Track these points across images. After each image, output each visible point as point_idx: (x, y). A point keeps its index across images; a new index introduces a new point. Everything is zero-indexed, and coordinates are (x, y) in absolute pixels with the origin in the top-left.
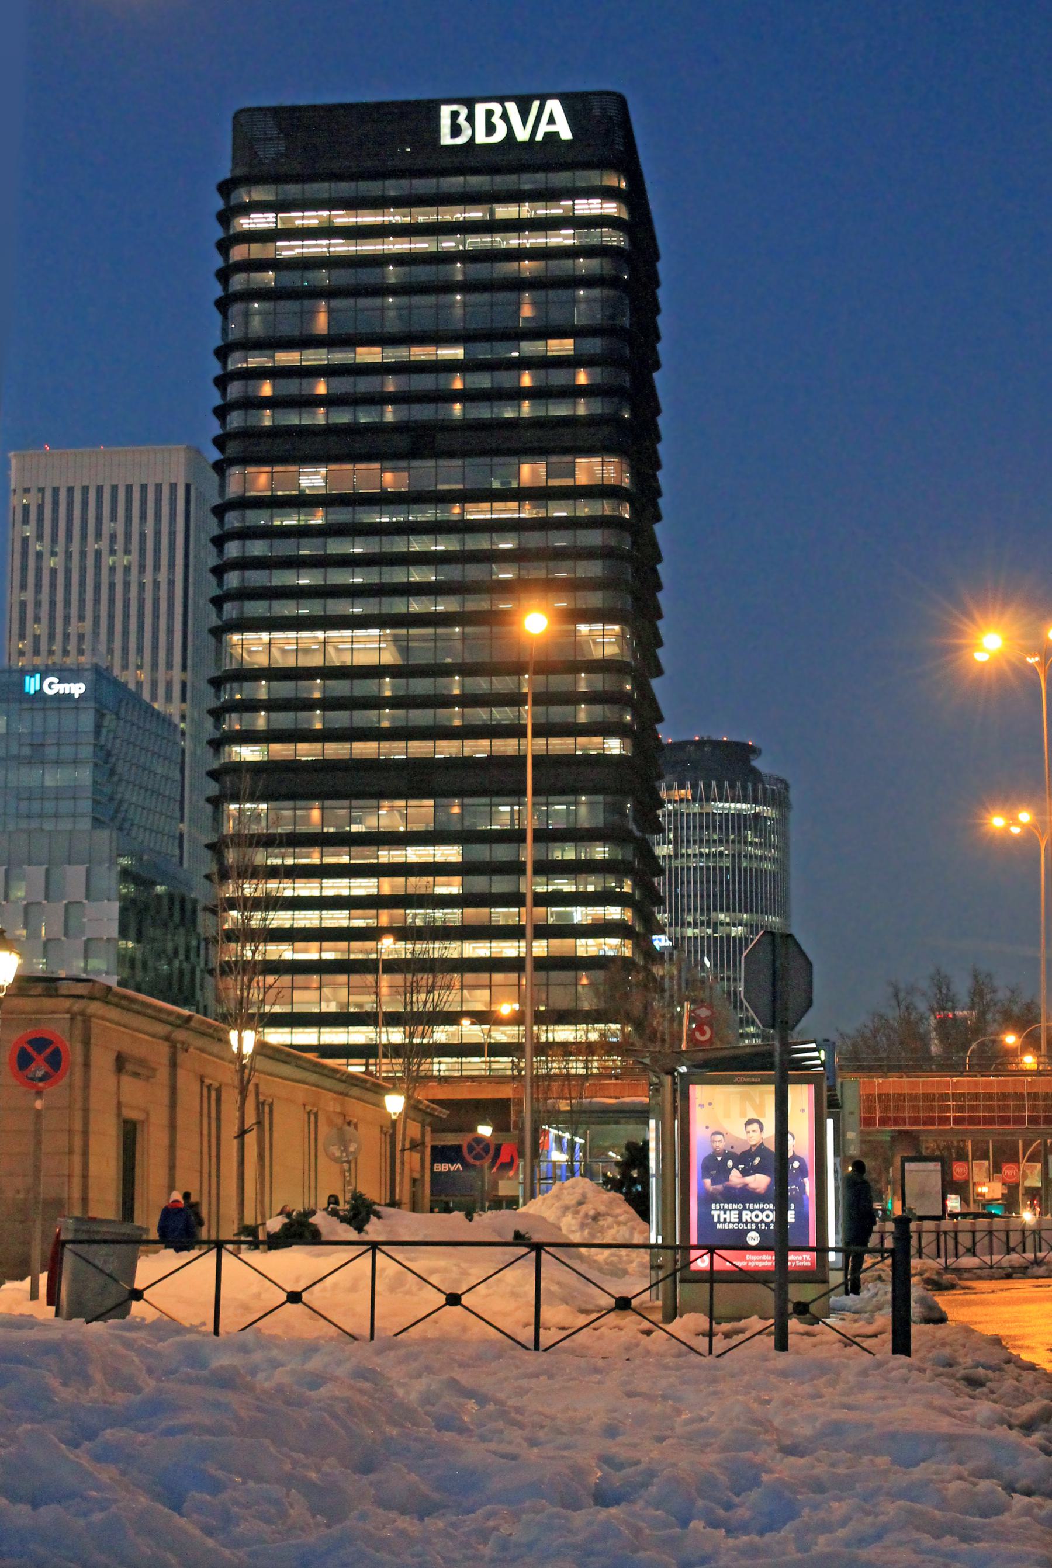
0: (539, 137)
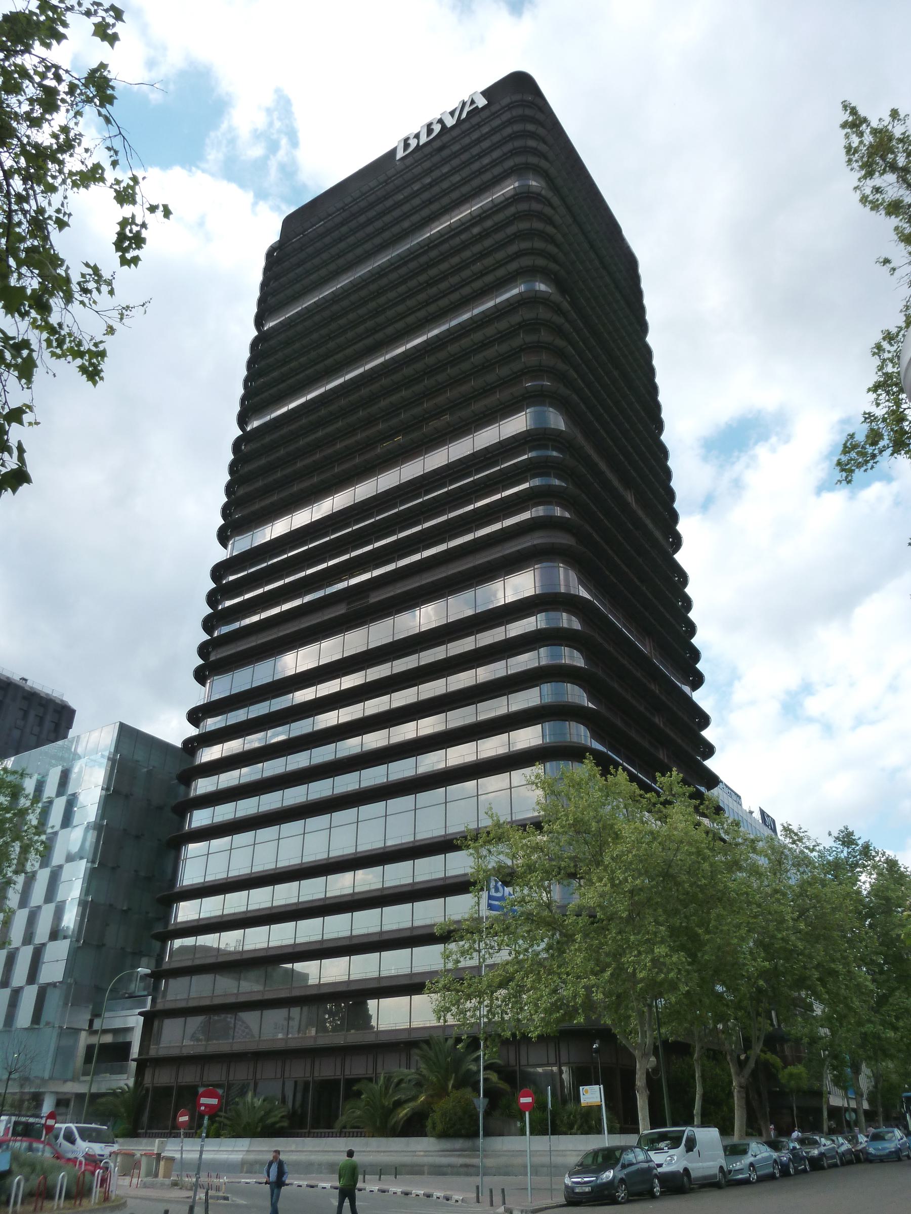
0: (464, 115)
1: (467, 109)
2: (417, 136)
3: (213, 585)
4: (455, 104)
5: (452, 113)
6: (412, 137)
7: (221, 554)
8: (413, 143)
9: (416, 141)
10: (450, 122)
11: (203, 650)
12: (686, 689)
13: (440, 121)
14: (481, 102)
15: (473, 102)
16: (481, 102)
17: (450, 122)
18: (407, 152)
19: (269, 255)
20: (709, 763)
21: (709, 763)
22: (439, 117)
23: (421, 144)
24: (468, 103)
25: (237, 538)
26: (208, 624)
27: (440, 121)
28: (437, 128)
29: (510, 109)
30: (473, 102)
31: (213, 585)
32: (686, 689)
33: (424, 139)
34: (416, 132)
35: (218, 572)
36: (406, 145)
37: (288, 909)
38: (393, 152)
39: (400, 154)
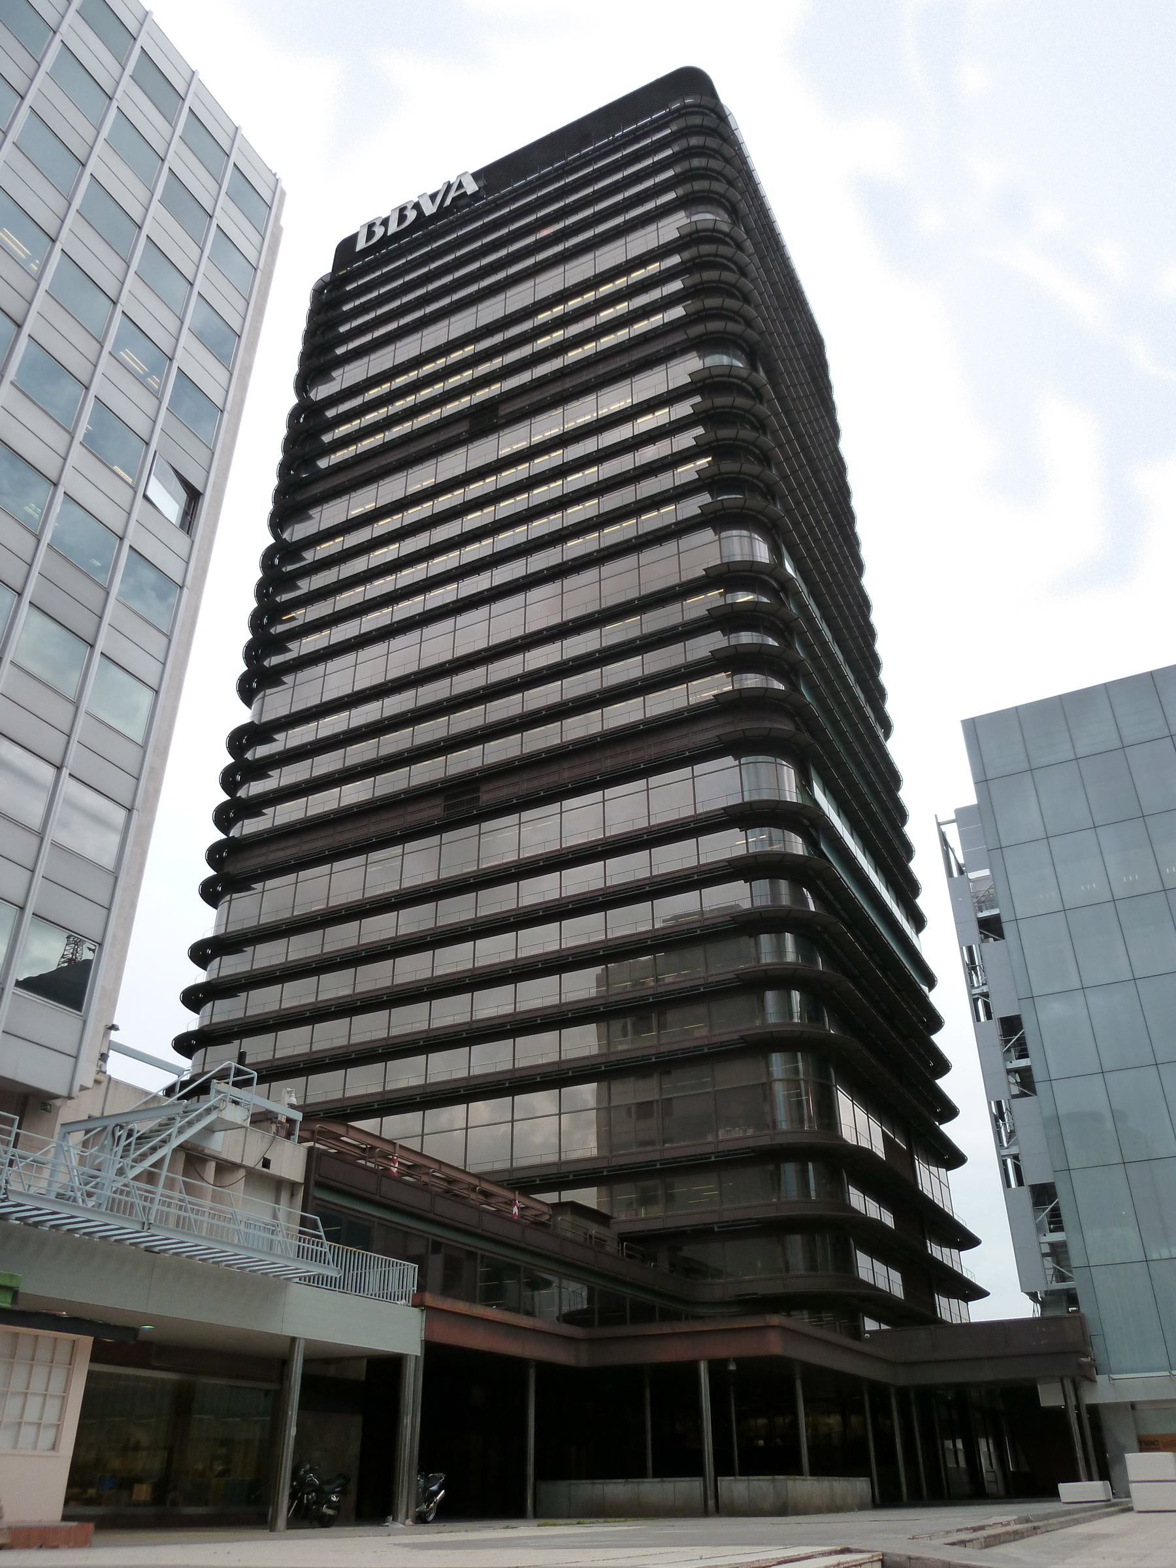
0: (448, 202)
1: (452, 194)
2: (385, 222)
3: (230, 760)
4: (438, 186)
5: (433, 197)
6: (378, 223)
7: (243, 715)
8: (379, 232)
9: (382, 229)
10: (429, 209)
11: (215, 855)
12: (925, 989)
13: (417, 206)
14: (471, 187)
15: (460, 186)
16: (471, 187)
17: (429, 209)
18: (403, 227)
19: (318, 292)
20: (947, 1128)
21: (947, 1128)
22: (416, 200)
23: (389, 234)
24: (455, 187)
25: (268, 691)
26: (223, 817)
27: (417, 206)
28: (411, 215)
29: (681, 116)
30: (460, 186)
31: (230, 760)
32: (925, 989)
33: (393, 228)
34: (384, 217)
35: (240, 740)
36: (402, 217)
37: (489, 1079)
38: (353, 239)
39: (361, 244)
